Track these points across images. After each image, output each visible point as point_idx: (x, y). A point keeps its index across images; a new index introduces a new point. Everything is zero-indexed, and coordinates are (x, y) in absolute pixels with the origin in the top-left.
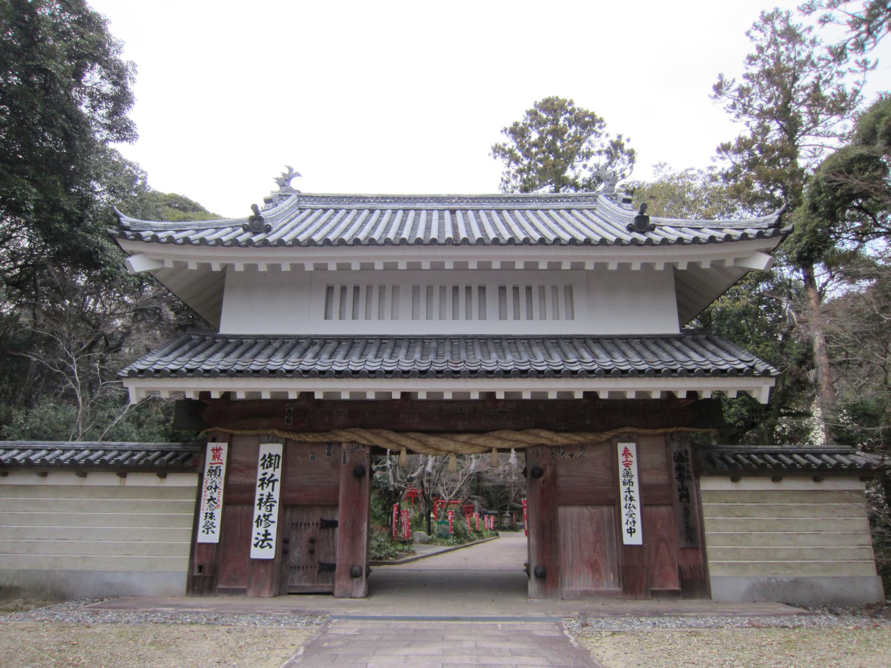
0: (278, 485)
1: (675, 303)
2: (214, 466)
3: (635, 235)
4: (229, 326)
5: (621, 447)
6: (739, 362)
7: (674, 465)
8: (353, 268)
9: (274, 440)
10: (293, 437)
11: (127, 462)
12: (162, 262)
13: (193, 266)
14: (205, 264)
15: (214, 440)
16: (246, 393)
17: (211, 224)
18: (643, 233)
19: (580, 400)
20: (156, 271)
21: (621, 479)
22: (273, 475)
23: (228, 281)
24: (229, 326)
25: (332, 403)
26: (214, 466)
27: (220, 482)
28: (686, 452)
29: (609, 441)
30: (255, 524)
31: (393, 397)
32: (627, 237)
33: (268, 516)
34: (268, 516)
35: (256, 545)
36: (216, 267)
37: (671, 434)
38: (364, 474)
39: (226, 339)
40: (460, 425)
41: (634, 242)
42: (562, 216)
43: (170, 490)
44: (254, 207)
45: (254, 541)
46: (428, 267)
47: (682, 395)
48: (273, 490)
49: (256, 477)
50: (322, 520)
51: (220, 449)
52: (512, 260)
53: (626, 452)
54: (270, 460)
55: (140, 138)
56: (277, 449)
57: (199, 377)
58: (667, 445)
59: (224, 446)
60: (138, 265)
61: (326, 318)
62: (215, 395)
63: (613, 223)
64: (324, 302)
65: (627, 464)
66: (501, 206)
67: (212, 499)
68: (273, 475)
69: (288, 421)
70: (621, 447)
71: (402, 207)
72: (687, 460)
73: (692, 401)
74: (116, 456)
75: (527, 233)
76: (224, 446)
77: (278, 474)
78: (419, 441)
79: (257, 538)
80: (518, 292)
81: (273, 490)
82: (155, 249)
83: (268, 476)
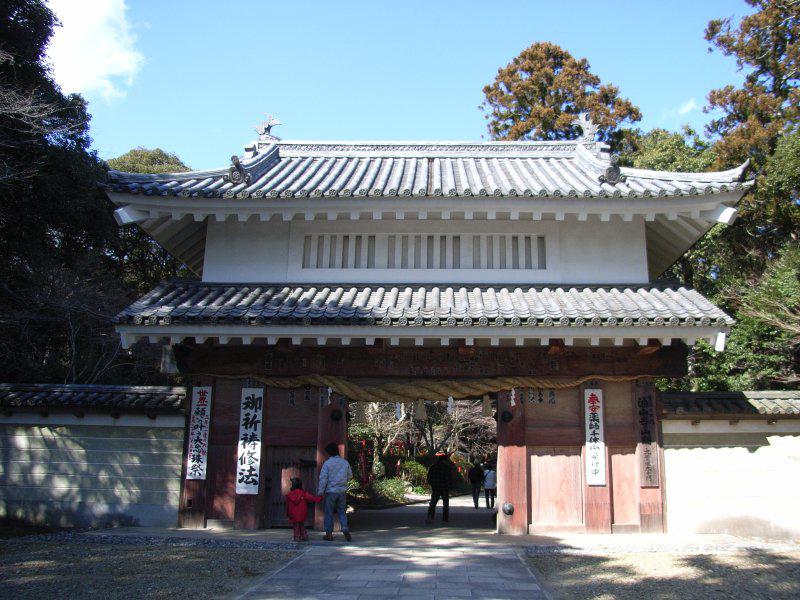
0: (259, 426)
1: (645, 250)
2: (201, 407)
3: (606, 186)
4: (209, 276)
5: (588, 393)
6: (698, 311)
7: (639, 409)
8: (466, 217)
9: (257, 385)
10: (270, 382)
11: (80, 403)
12: (148, 212)
13: (177, 216)
14: (187, 215)
15: (199, 385)
16: (500, 340)
17: (191, 175)
18: (613, 184)
19: (446, 347)
20: (142, 222)
21: (588, 423)
22: (255, 416)
23: (210, 229)
24: (209, 276)
25: (309, 348)
26: (201, 407)
27: (206, 419)
28: (650, 397)
29: (578, 387)
30: (239, 462)
31: (319, 343)
32: (596, 189)
33: (252, 454)
34: (252, 454)
35: (240, 481)
36: (199, 218)
37: (637, 381)
38: (341, 416)
39: (210, 286)
40: (434, 371)
41: (604, 196)
42: (539, 166)
43: (88, 428)
44: (234, 158)
45: (239, 477)
46: (494, 217)
47: (370, 342)
48: (255, 430)
49: (238, 420)
50: (301, 460)
51: (205, 392)
52: (439, 211)
53: (593, 399)
54: (252, 403)
55: (77, 92)
56: (259, 393)
57: (291, 324)
58: (633, 391)
59: (209, 389)
60: (125, 216)
61: (303, 267)
62: (199, 341)
63: (588, 173)
64: (301, 256)
65: (594, 409)
66: (480, 154)
67: (198, 440)
68: (255, 416)
69: (268, 367)
70: (588, 393)
71: (380, 155)
72: (651, 405)
73: (656, 349)
74: (110, 398)
75: (542, 184)
76: (209, 389)
77: (260, 415)
78: (448, 386)
79: (241, 474)
80: (433, 241)
81: (255, 430)
82: (143, 201)
83: (251, 417)
